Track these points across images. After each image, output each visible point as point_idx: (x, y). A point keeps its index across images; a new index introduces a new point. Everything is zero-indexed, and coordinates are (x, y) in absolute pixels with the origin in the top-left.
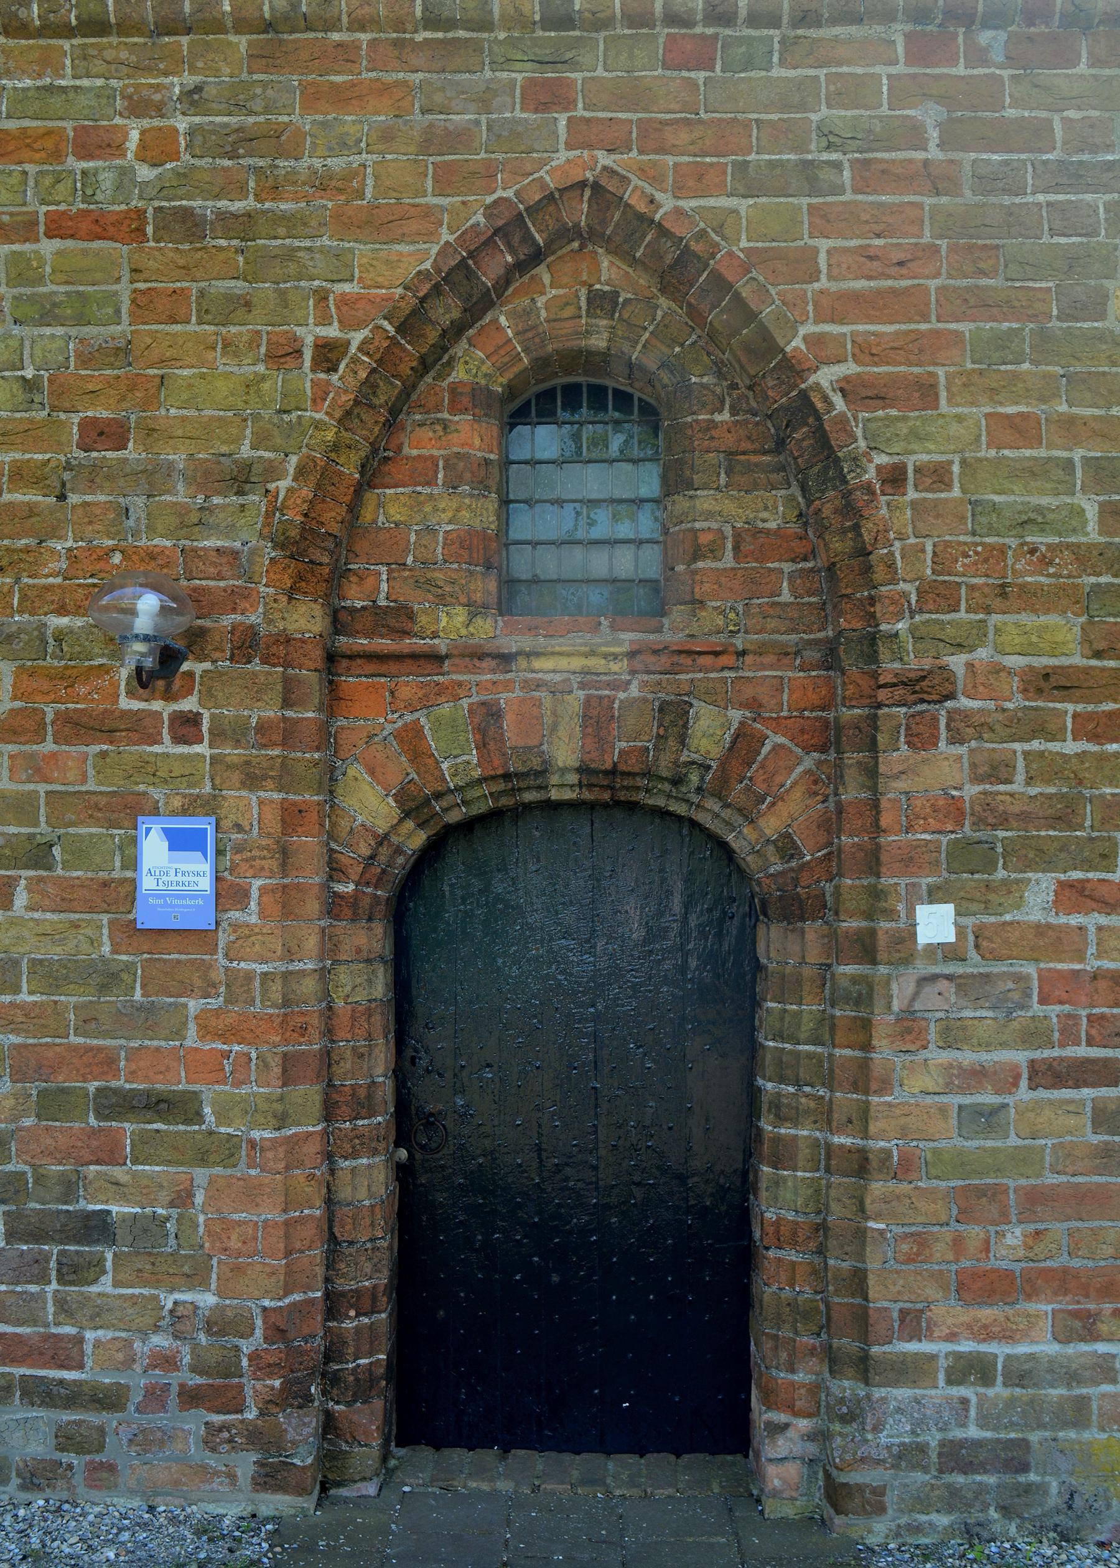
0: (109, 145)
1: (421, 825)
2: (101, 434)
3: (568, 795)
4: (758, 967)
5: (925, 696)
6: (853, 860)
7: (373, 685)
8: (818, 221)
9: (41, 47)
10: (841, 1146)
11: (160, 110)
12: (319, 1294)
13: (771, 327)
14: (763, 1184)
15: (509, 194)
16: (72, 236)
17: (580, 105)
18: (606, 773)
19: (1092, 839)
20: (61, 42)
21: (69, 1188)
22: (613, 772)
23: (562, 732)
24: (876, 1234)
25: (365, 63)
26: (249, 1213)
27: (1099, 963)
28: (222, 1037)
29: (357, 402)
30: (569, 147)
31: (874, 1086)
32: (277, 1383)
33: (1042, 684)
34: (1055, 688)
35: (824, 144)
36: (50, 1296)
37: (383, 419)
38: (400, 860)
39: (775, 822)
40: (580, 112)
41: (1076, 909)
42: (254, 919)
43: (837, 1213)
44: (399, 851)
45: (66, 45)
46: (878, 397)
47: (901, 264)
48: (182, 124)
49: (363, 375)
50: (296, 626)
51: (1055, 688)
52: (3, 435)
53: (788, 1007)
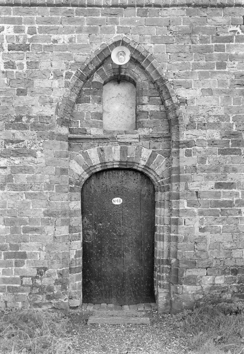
0: (21, 30)
1: (88, 173)
2: (21, 92)
3: (117, 166)
4: (155, 202)
5: (189, 146)
6: (175, 175)
7: (78, 144)
8: (168, 49)
9: (6, 8)
10: (172, 236)
11: (32, 23)
12: (69, 268)
13: (158, 71)
14: (158, 228)
15: (105, 43)
16: (14, 50)
17: (120, 24)
18: (125, 162)
19: (222, 174)
20: (11, 7)
21: (17, 247)
22: (127, 162)
23: (116, 154)
24: (180, 253)
25: (75, 14)
26: (56, 245)
27: (223, 199)
28: (48, 216)
29: (74, 86)
30: (117, 33)
31: (179, 223)
32: (60, 286)
33: (212, 143)
34: (215, 144)
35: (170, 32)
36: (13, 270)
37: (79, 89)
38: (83, 180)
39: (159, 170)
40: (120, 25)
41: (219, 188)
42: (55, 192)
43: (172, 249)
44: (83, 178)
45: (12, 8)
46: (180, 85)
47: (185, 58)
48: (37, 26)
49: (76, 80)
50: (62, 132)
51: (215, 144)
52: (1, 92)
53: (164, 266)
